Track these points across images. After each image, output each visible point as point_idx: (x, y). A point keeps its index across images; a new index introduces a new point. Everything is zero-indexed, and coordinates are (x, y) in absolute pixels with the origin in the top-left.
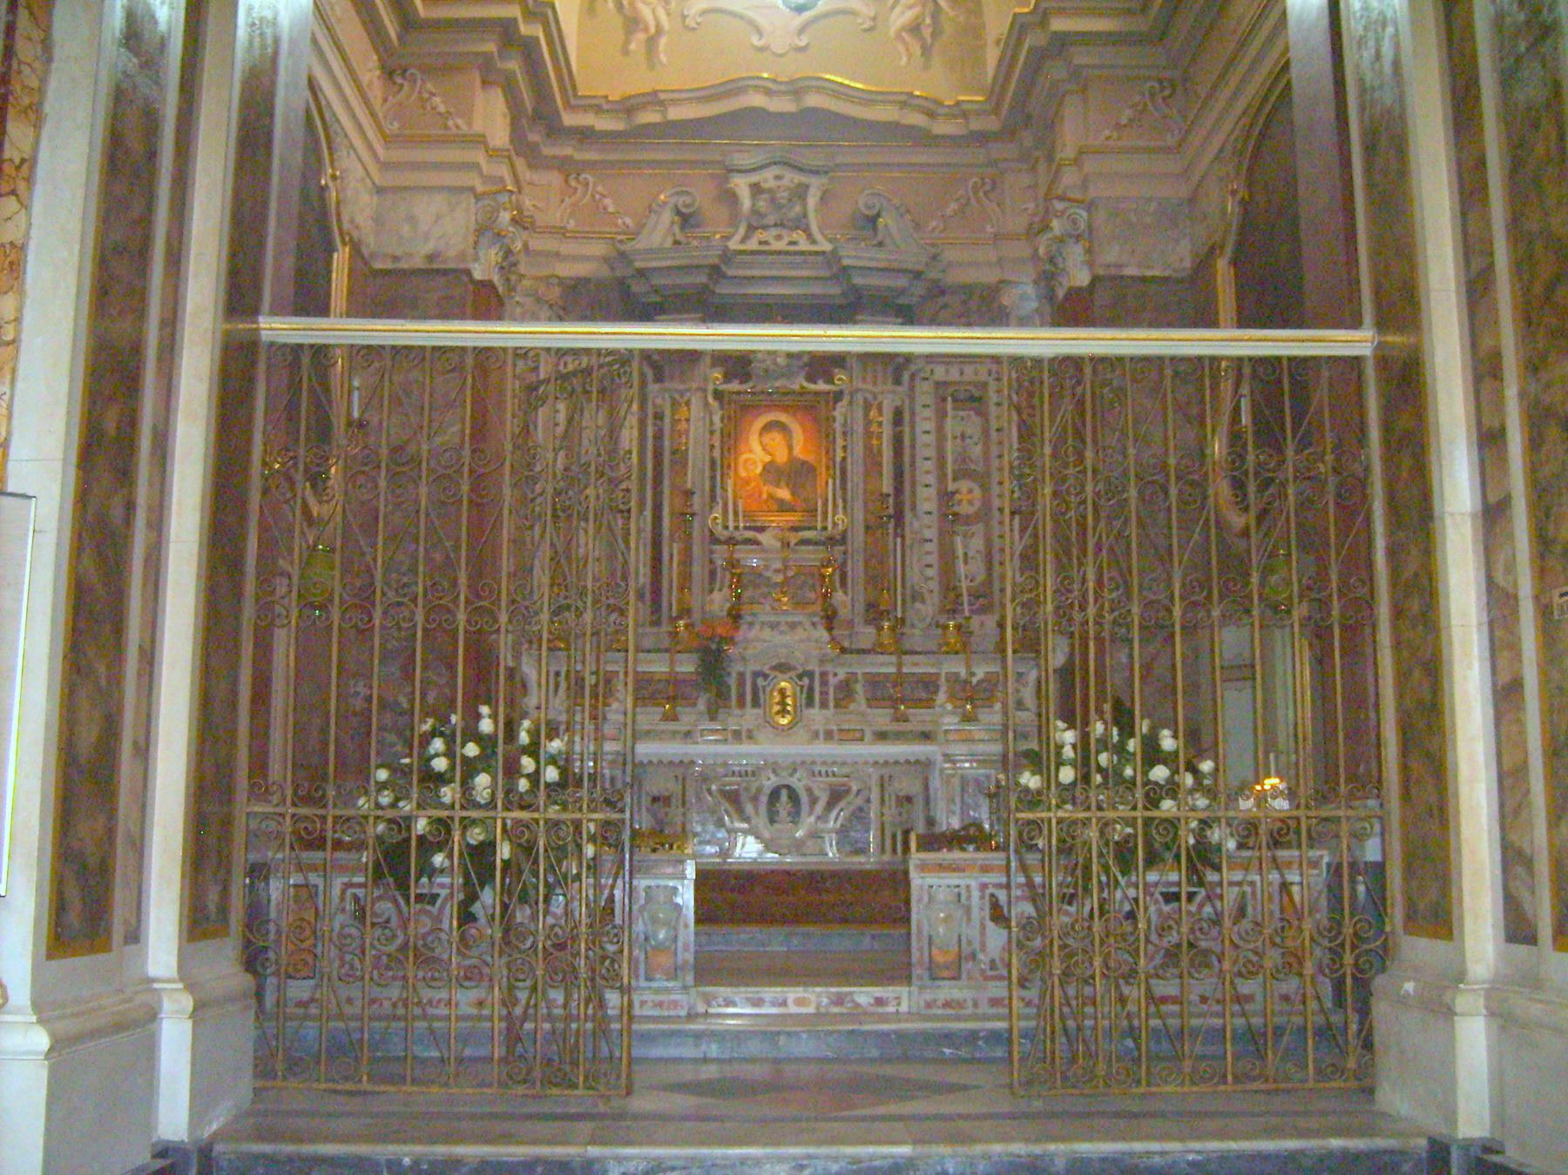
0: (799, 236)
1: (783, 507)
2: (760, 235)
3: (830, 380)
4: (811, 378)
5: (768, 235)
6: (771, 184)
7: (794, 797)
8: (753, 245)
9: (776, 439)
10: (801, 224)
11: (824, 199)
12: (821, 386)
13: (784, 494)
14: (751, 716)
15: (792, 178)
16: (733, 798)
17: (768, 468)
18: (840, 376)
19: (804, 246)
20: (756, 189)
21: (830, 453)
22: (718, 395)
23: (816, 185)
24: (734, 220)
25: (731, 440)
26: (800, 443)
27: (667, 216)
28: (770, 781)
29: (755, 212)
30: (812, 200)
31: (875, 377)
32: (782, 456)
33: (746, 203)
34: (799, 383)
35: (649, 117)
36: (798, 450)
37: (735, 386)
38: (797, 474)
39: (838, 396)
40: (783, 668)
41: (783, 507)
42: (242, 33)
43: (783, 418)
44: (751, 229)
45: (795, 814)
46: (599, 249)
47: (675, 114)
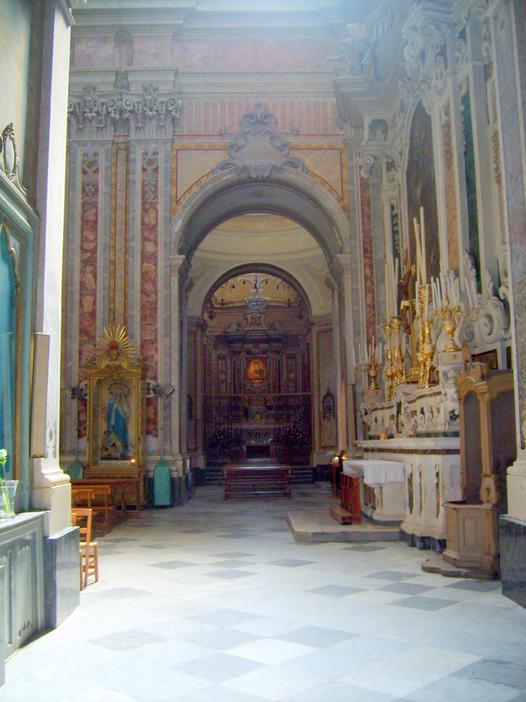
0: (260, 327)
1: (258, 379)
2: (253, 327)
3: (266, 354)
4: (263, 354)
5: (254, 326)
6: (254, 316)
7: (259, 434)
8: (251, 328)
9: (256, 365)
10: (260, 324)
11: (264, 318)
12: (264, 356)
13: (258, 375)
14: (252, 421)
15: (258, 315)
16: (250, 434)
17: (255, 371)
18: (268, 354)
19: (261, 329)
20: (252, 318)
21: (266, 368)
22: (246, 358)
23: (263, 316)
24: (247, 323)
25: (248, 366)
26: (261, 366)
27: (235, 325)
28: (255, 432)
29: (251, 322)
30: (262, 319)
31: (180, 482)
32: (257, 369)
33: (250, 320)
34: (261, 355)
35: (231, 305)
36: (261, 368)
37: (248, 356)
38: (260, 372)
39: (268, 358)
40: (257, 413)
41: (258, 379)
42: (458, 558)
43: (258, 361)
44: (251, 326)
45: (260, 437)
46: (222, 330)
47: (236, 305)
